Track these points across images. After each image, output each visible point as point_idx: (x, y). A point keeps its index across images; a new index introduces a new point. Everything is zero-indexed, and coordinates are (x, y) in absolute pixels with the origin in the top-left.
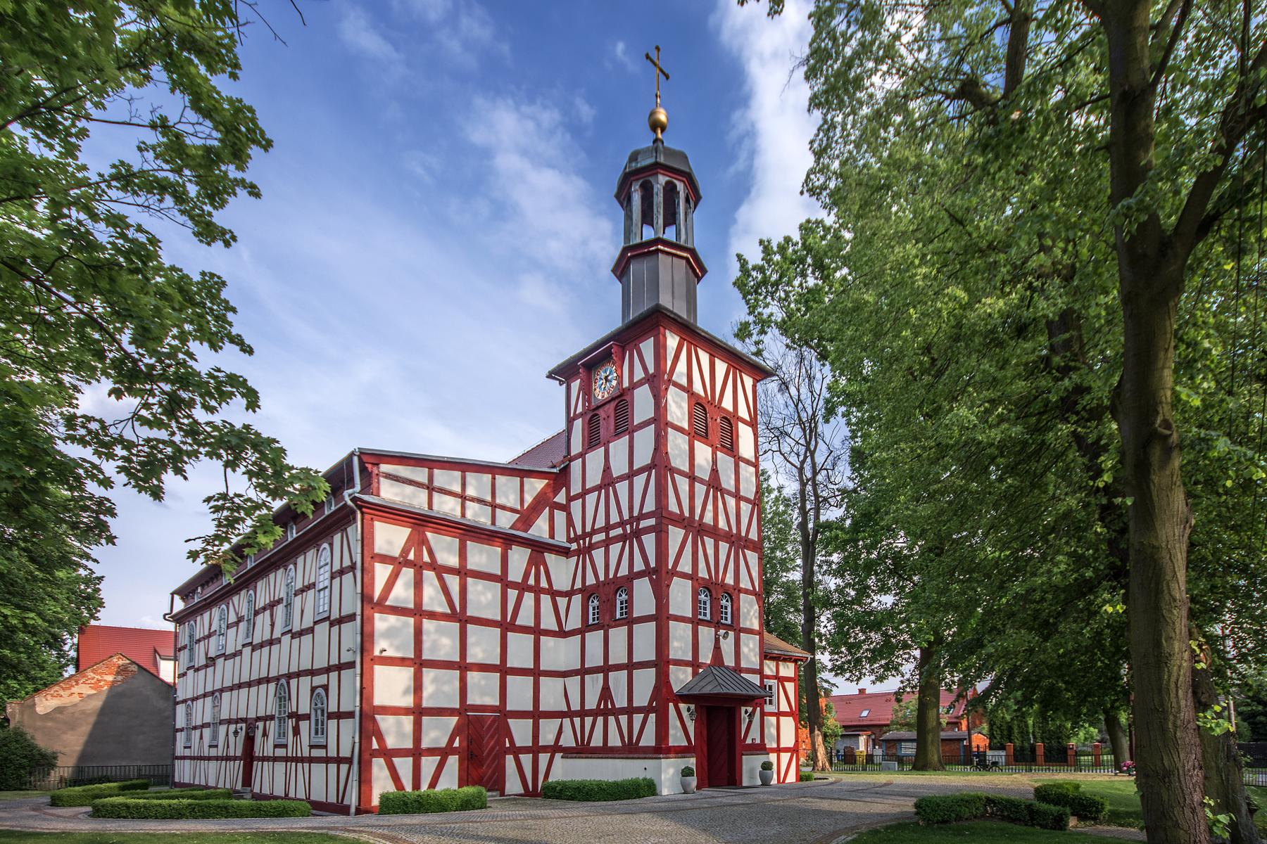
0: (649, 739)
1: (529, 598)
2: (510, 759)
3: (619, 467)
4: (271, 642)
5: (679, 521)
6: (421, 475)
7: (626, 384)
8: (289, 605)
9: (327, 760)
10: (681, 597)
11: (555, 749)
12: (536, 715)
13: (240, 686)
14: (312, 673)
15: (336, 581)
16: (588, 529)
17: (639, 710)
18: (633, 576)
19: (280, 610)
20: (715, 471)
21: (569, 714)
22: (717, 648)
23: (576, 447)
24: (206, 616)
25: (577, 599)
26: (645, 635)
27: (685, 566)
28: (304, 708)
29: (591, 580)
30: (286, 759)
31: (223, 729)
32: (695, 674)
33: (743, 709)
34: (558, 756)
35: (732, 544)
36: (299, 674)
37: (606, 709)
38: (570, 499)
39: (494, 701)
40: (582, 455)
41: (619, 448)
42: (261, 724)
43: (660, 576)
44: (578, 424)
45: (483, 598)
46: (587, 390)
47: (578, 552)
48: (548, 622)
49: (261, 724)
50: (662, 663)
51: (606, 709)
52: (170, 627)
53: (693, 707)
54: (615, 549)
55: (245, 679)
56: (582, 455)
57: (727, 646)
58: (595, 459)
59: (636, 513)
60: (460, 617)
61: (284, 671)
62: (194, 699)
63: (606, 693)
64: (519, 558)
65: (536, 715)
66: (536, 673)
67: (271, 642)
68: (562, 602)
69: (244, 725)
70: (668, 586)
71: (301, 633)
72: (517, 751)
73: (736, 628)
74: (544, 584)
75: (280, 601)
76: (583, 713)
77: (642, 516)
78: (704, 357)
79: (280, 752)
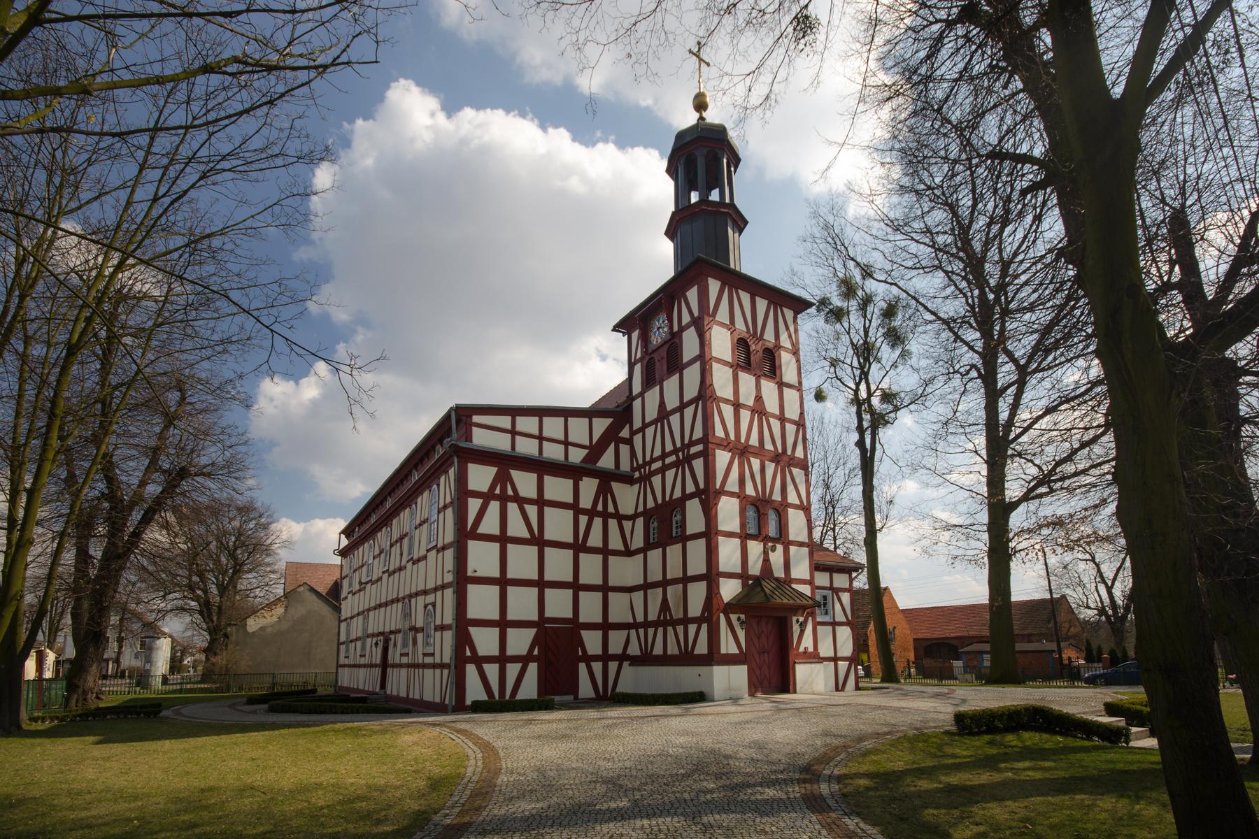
0: (702, 648)
1: (598, 522)
2: (582, 667)
3: (672, 402)
4: (401, 569)
6: (505, 422)
7: (676, 328)
8: (411, 539)
9: (434, 666)
10: (728, 513)
11: (623, 658)
12: (605, 626)
13: (380, 606)
14: (425, 593)
15: (441, 515)
16: (648, 459)
17: (694, 620)
18: (686, 497)
19: (406, 541)
20: (759, 398)
21: (634, 625)
22: (766, 560)
23: (637, 388)
25: (640, 522)
26: (697, 549)
27: (732, 485)
28: (420, 624)
30: (408, 666)
31: (369, 640)
32: (744, 585)
33: (794, 619)
34: (626, 664)
36: (417, 594)
37: (665, 621)
38: (633, 433)
39: (569, 614)
40: (641, 394)
41: (671, 384)
42: (392, 637)
43: (708, 496)
44: (638, 368)
45: (559, 525)
46: (645, 338)
47: (639, 480)
48: (615, 543)
49: (392, 637)
50: (712, 576)
51: (665, 621)
52: (337, 560)
53: (743, 617)
54: (670, 474)
55: (383, 600)
56: (641, 394)
57: (777, 557)
58: (653, 396)
59: (686, 441)
60: (538, 541)
61: (407, 592)
62: (352, 618)
63: (665, 606)
64: (589, 487)
65: (605, 626)
66: (605, 589)
67: (401, 569)
68: (627, 525)
70: (716, 504)
71: (419, 560)
72: (589, 659)
73: (782, 537)
75: (406, 535)
76: (646, 624)
77: (693, 443)
78: (745, 297)
79: (404, 660)
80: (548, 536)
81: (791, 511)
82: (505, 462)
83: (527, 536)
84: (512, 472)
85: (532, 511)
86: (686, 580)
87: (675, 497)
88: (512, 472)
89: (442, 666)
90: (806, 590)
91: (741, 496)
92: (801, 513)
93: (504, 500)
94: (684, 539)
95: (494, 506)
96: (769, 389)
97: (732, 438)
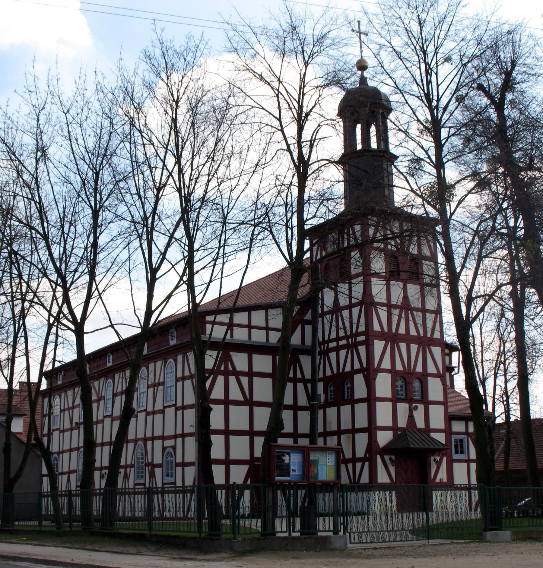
0: (365, 479)
3: (343, 301)
5: (382, 336)
10: (383, 385)
18: (354, 372)
20: (406, 297)
22: (411, 417)
24: (70, 393)
26: (362, 409)
27: (386, 364)
28: (158, 460)
29: (328, 373)
33: (432, 458)
35: (420, 344)
43: (370, 373)
50: (371, 429)
53: (393, 457)
54: (343, 353)
60: (249, 402)
69: (107, 471)
70: (375, 379)
73: (426, 402)
74: (299, 376)
77: (358, 334)
80: (256, 398)
81: (430, 380)
82: (226, 348)
83: (242, 399)
84: (231, 353)
85: (245, 380)
86: (354, 431)
87: (346, 370)
88: (231, 353)
89: (184, 490)
90: (441, 438)
91: (392, 371)
92: (438, 380)
93: (226, 374)
94: (353, 402)
95: (220, 379)
96: (413, 290)
97: (386, 330)
